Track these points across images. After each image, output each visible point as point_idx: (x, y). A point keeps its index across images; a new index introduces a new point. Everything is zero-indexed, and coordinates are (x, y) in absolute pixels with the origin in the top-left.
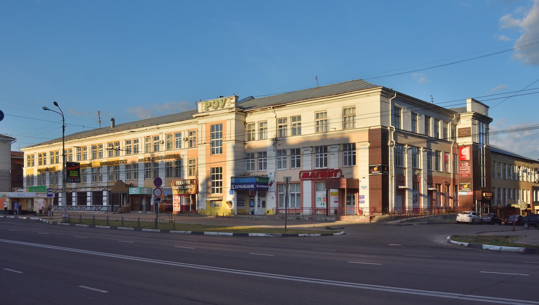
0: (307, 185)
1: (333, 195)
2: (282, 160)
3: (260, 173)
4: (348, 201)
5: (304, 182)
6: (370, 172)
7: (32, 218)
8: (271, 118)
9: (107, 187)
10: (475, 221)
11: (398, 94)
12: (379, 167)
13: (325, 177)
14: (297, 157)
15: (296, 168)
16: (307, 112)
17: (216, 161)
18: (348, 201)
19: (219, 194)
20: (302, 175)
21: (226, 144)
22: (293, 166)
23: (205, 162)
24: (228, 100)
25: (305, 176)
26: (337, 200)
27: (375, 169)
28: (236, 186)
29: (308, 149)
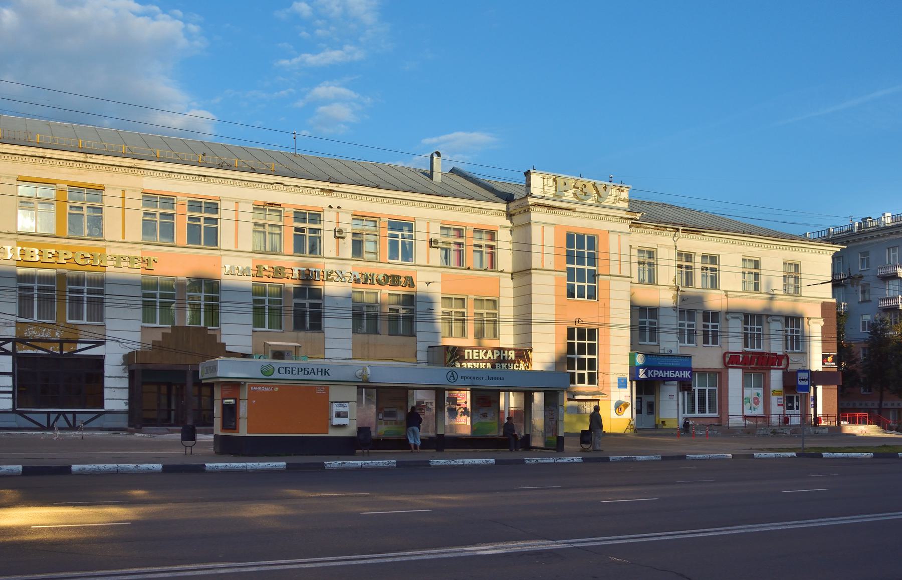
0: (735, 376)
1: (776, 395)
2: (710, 329)
3: (495, 344)
4: (790, 405)
5: (730, 370)
6: (823, 364)
7: (434, 462)
8: (669, 247)
9: (15, 341)
10: (501, 416)
11: (217, 228)
12: (834, 357)
13: (756, 364)
14: (683, 325)
15: (710, 345)
16: (731, 253)
17: (583, 312)
18: (790, 405)
19: (593, 388)
20: (727, 360)
21: (608, 282)
22: (706, 341)
23: (552, 318)
24: (613, 192)
25: (732, 360)
26: (781, 402)
27: (830, 359)
28: (650, 373)
29: (737, 315)
